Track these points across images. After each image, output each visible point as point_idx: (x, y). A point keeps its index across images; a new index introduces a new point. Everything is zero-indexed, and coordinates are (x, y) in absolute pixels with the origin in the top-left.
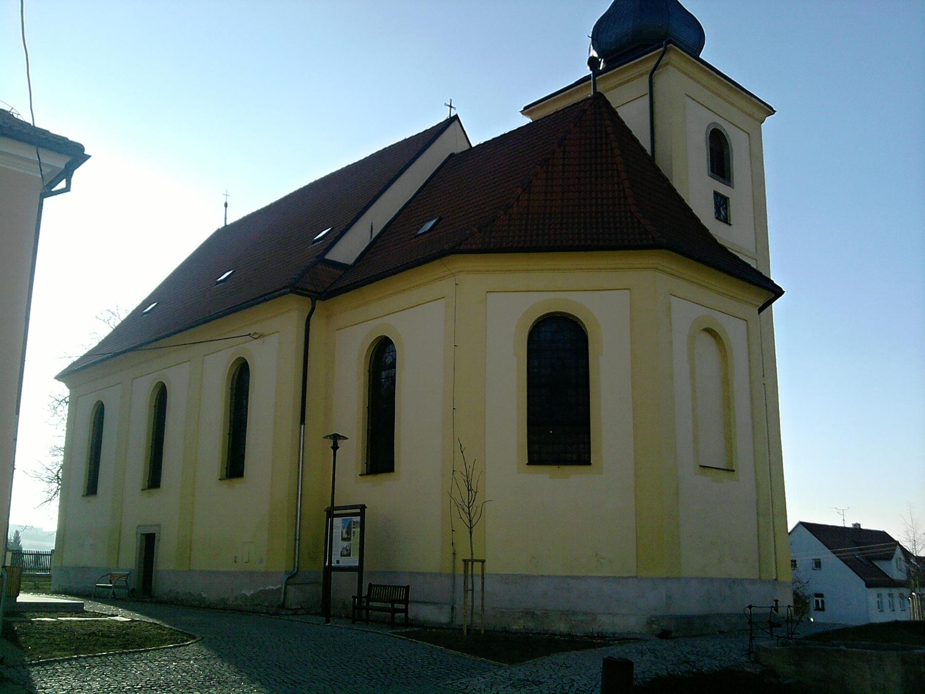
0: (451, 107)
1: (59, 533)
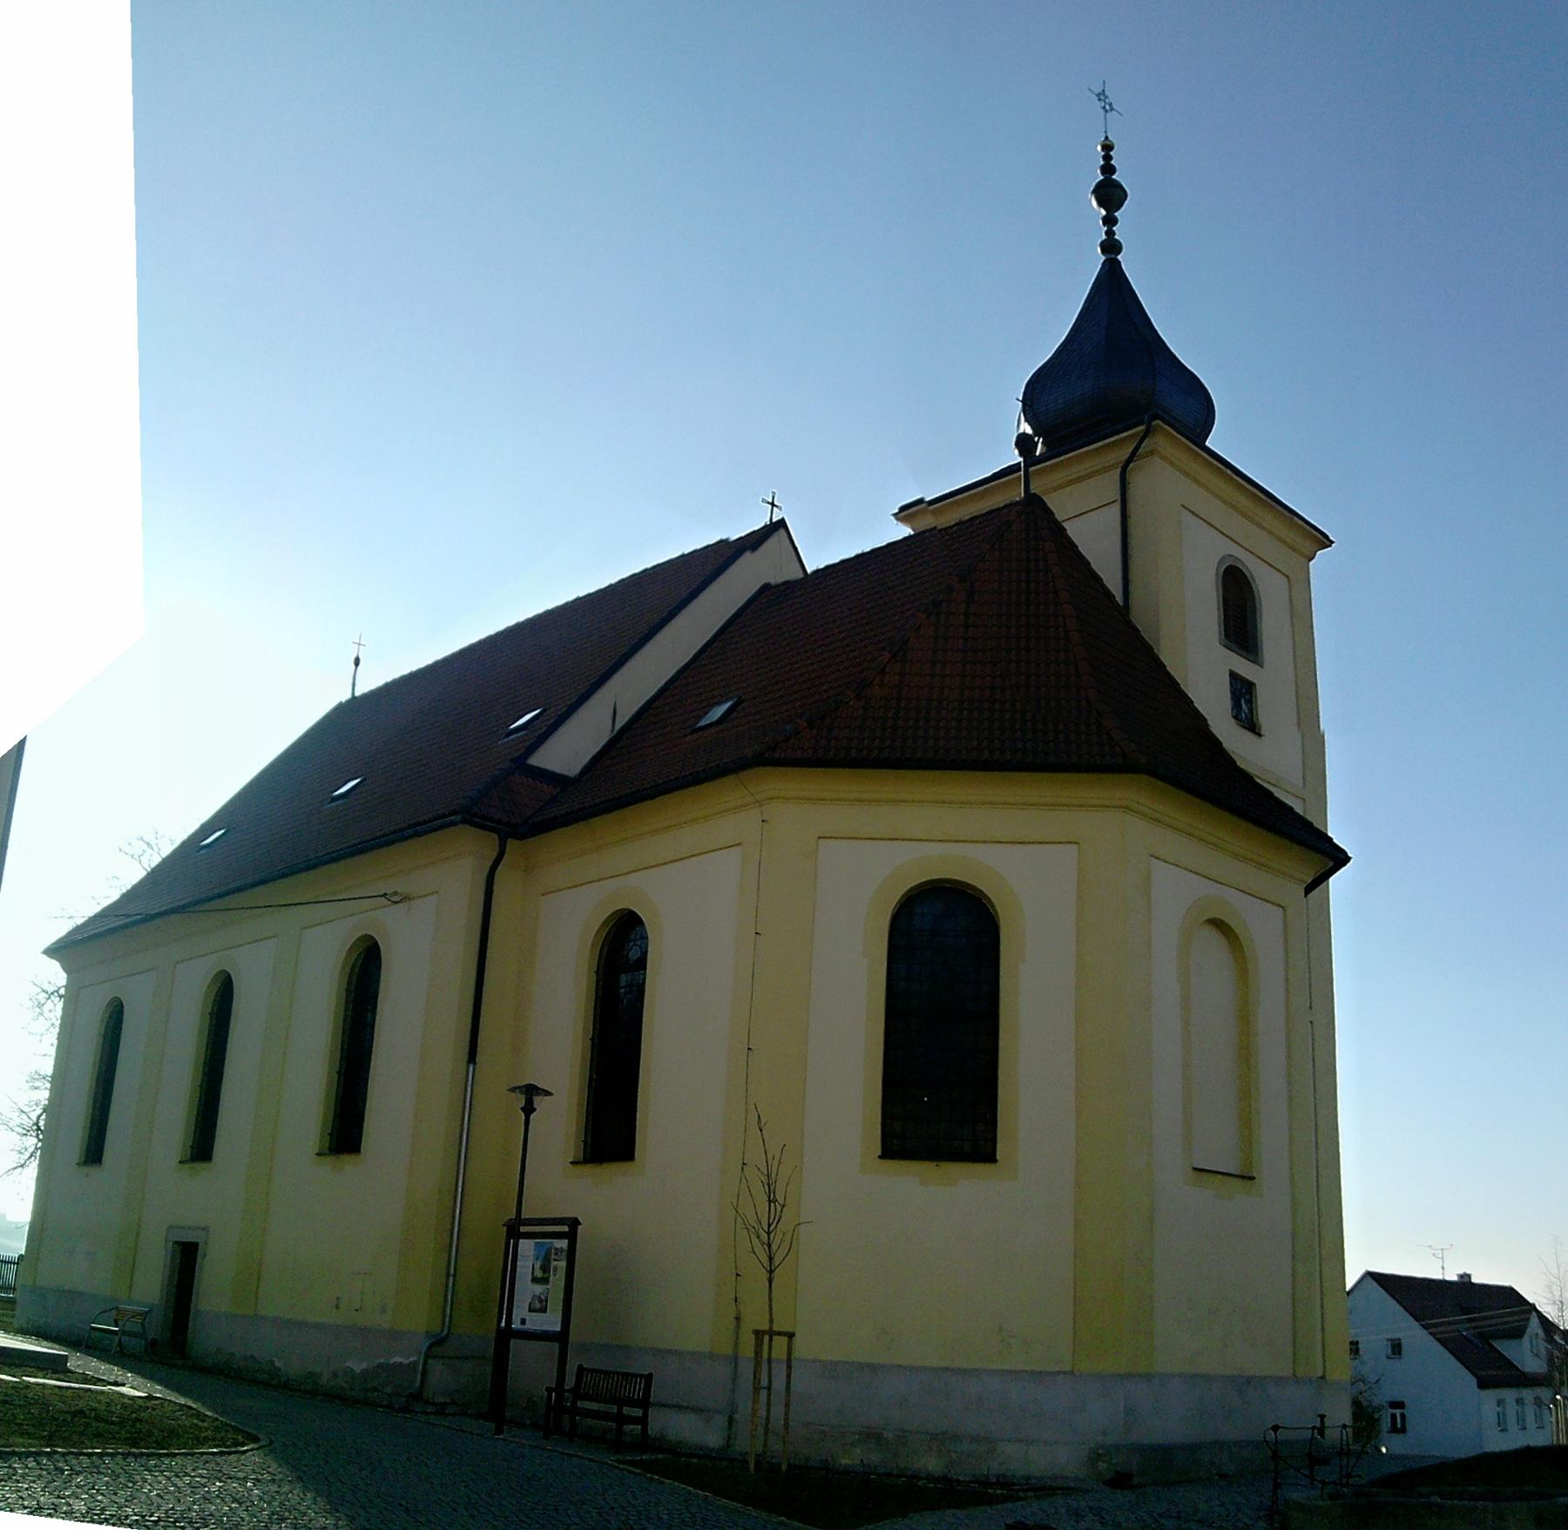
0: (773, 505)
1: (34, 1226)
